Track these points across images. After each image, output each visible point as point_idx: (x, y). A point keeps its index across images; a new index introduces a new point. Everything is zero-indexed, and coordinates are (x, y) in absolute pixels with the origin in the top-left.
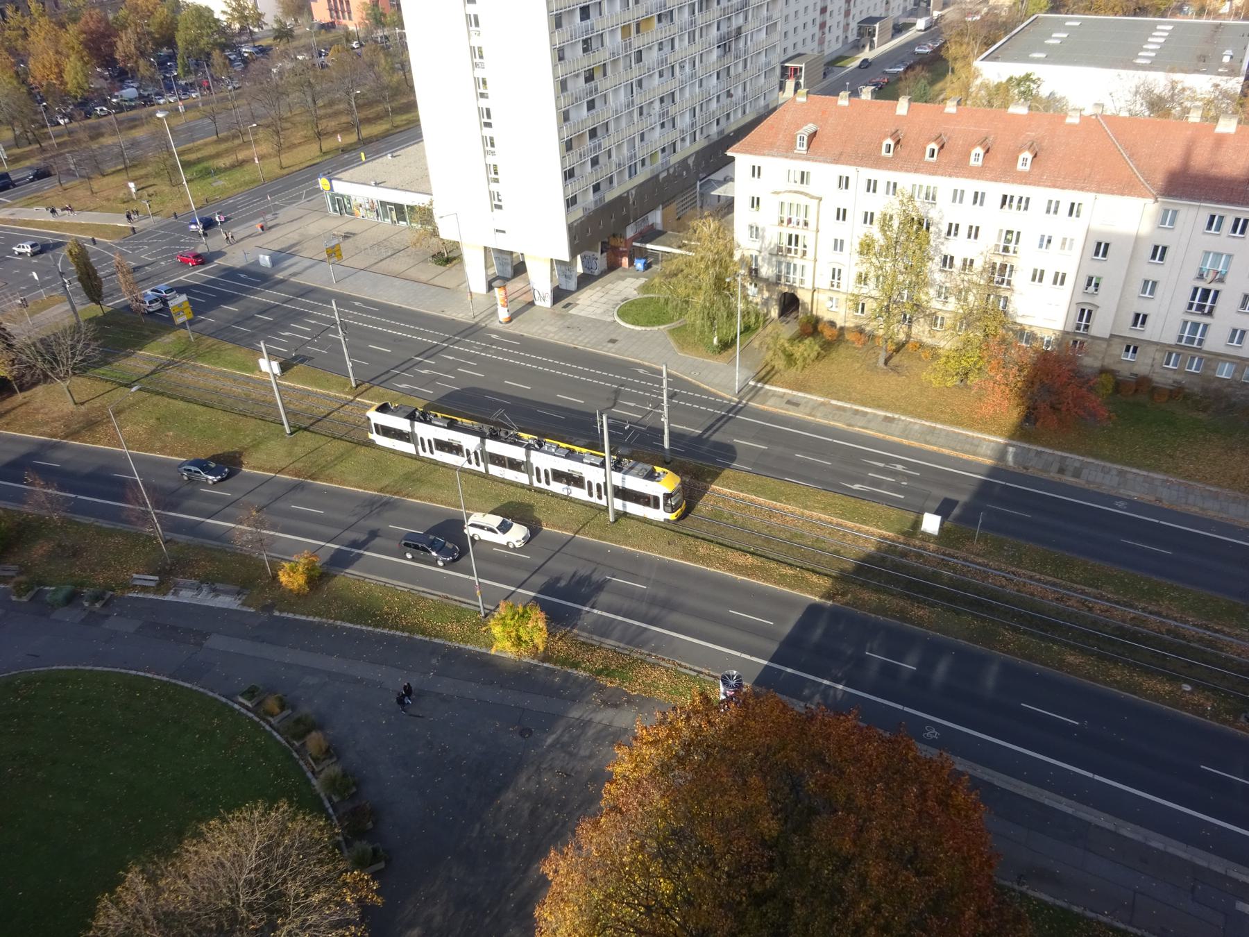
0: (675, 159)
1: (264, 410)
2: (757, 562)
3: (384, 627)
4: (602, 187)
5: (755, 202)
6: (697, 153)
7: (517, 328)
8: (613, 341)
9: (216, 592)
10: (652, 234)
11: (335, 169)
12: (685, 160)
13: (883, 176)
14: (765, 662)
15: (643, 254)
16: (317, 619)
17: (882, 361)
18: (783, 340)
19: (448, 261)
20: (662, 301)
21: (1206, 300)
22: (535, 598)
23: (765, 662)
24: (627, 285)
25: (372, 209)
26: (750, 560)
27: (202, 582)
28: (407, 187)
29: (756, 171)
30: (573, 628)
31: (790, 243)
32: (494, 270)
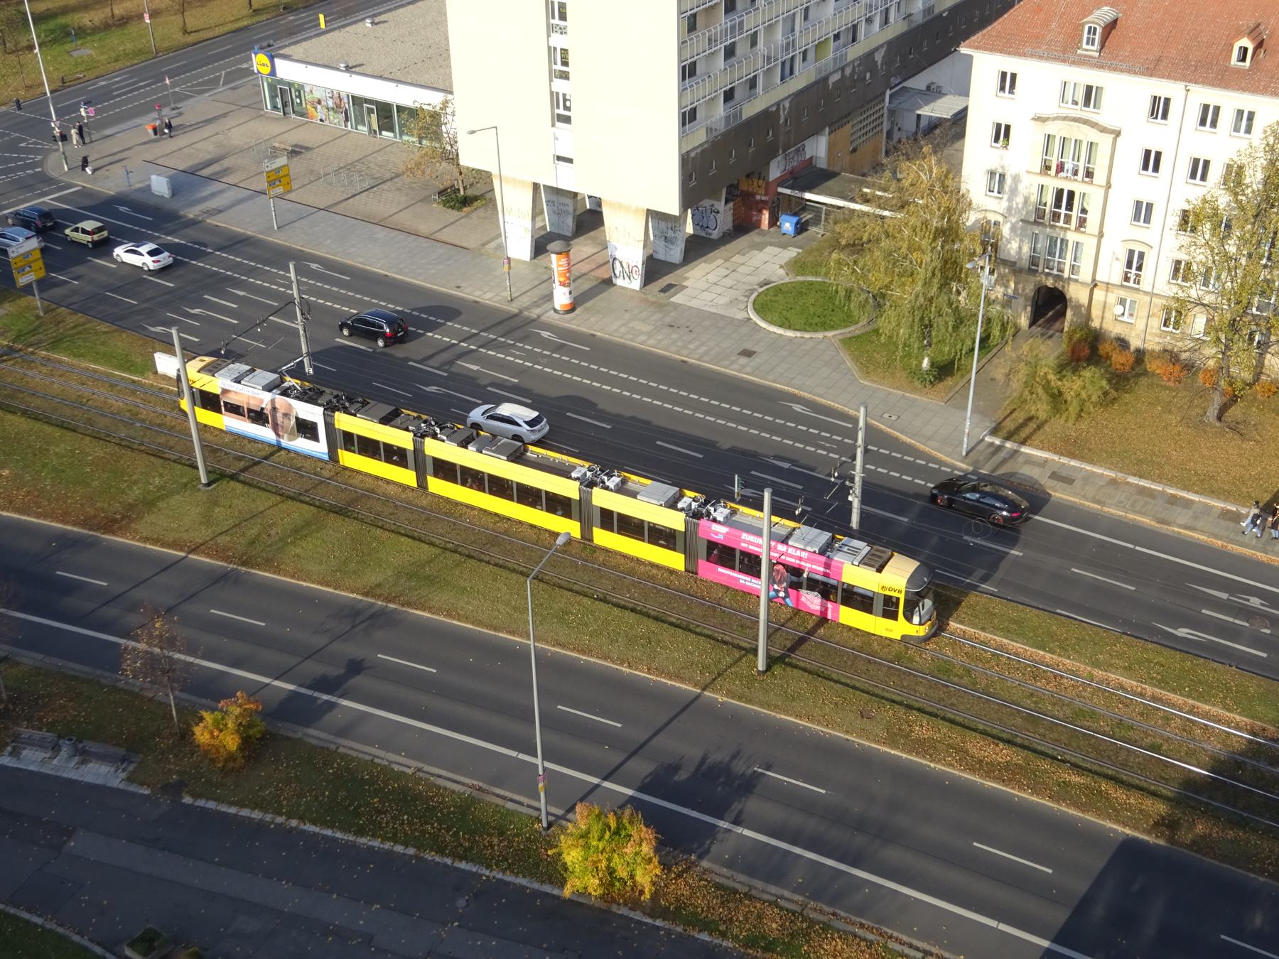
0: (854, 52)
1: (162, 439)
2: (1018, 757)
3: (374, 836)
4: (737, 95)
5: (1002, 133)
6: (889, 43)
7: (586, 323)
8: (748, 353)
9: (85, 756)
10: (814, 177)
11: (277, 37)
12: (871, 54)
13: (1230, 101)
14: (1045, 944)
15: (800, 207)
16: (256, 815)
17: (1213, 411)
18: (1047, 369)
19: (466, 201)
20: (842, 293)
21: (1059, 207)
22: (632, 799)
23: (1045, 944)
24: (767, 259)
25: (337, 108)
26: (1003, 754)
27: (60, 737)
28: (398, 75)
29: (1007, 82)
30: (700, 857)
31: (1058, 204)
32: (546, 220)
